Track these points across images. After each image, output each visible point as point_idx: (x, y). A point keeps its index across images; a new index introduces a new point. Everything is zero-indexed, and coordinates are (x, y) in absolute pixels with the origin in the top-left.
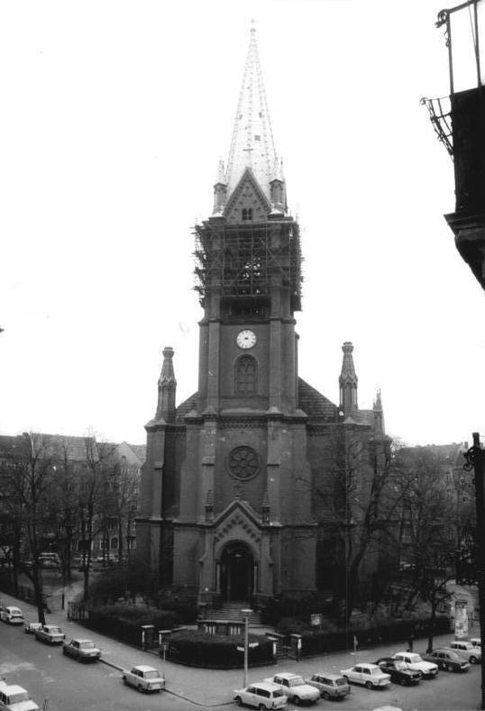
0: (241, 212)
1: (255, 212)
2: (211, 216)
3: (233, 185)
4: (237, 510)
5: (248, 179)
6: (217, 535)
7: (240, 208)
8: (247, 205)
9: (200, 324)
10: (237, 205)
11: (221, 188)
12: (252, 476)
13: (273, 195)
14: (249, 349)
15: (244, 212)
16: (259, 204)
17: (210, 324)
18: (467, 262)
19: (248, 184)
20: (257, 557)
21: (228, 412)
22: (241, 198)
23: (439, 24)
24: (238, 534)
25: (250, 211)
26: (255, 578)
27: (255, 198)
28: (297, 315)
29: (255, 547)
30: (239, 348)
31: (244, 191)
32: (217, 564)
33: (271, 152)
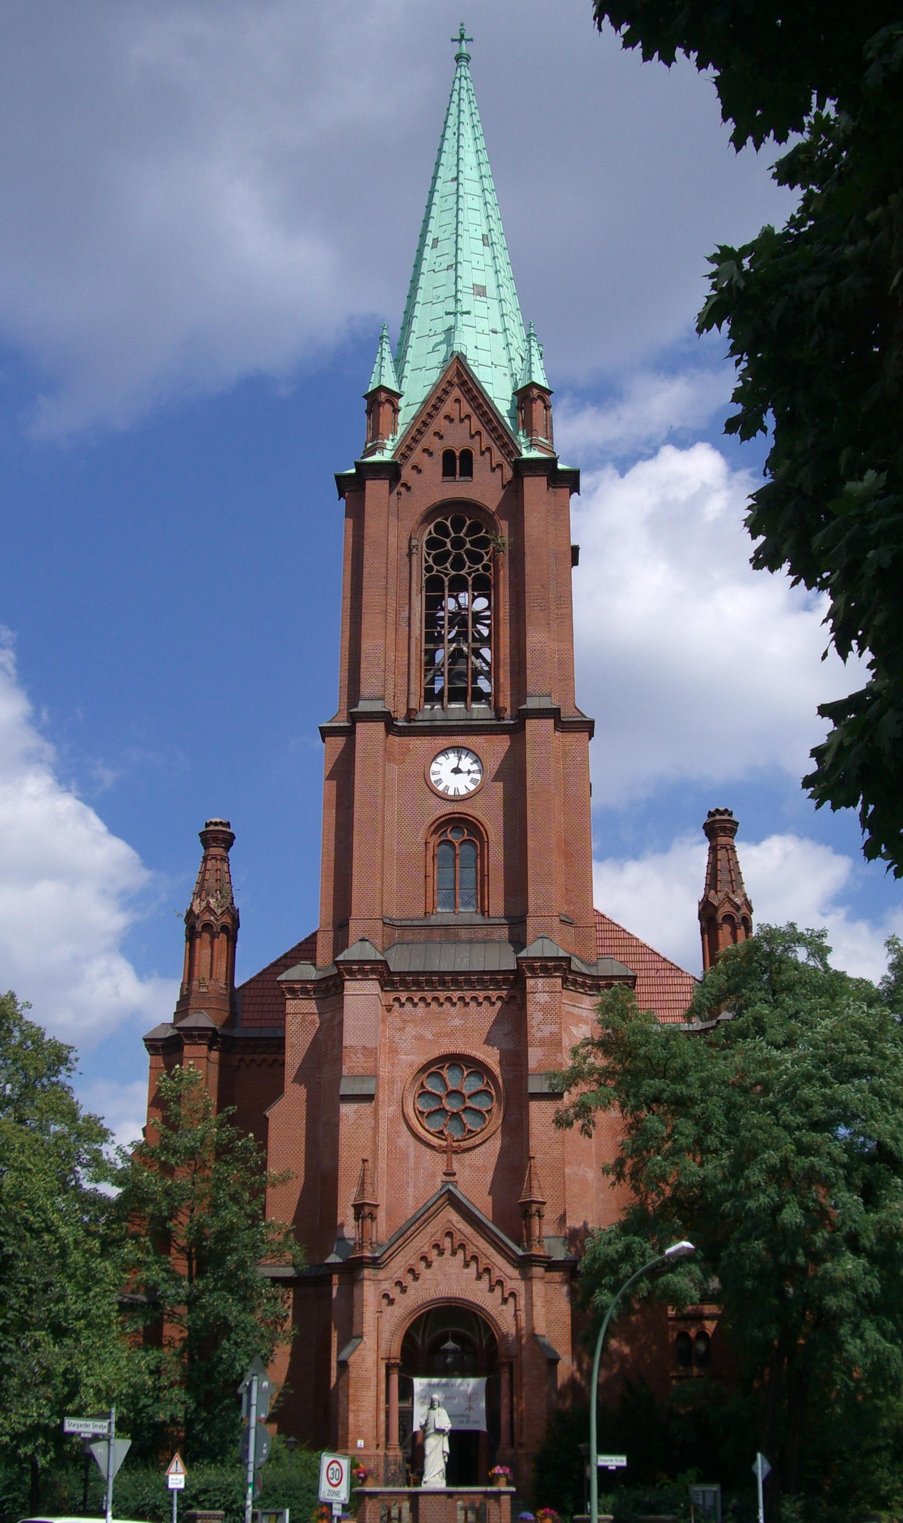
6: (387, 1286)
7: (439, 447)
8: (457, 438)
10: (428, 440)
15: (448, 456)
16: (487, 440)
17: (361, 728)
19: (456, 392)
21: (398, 962)
22: (438, 423)
25: (467, 456)
27: (476, 424)
32: (388, 1367)
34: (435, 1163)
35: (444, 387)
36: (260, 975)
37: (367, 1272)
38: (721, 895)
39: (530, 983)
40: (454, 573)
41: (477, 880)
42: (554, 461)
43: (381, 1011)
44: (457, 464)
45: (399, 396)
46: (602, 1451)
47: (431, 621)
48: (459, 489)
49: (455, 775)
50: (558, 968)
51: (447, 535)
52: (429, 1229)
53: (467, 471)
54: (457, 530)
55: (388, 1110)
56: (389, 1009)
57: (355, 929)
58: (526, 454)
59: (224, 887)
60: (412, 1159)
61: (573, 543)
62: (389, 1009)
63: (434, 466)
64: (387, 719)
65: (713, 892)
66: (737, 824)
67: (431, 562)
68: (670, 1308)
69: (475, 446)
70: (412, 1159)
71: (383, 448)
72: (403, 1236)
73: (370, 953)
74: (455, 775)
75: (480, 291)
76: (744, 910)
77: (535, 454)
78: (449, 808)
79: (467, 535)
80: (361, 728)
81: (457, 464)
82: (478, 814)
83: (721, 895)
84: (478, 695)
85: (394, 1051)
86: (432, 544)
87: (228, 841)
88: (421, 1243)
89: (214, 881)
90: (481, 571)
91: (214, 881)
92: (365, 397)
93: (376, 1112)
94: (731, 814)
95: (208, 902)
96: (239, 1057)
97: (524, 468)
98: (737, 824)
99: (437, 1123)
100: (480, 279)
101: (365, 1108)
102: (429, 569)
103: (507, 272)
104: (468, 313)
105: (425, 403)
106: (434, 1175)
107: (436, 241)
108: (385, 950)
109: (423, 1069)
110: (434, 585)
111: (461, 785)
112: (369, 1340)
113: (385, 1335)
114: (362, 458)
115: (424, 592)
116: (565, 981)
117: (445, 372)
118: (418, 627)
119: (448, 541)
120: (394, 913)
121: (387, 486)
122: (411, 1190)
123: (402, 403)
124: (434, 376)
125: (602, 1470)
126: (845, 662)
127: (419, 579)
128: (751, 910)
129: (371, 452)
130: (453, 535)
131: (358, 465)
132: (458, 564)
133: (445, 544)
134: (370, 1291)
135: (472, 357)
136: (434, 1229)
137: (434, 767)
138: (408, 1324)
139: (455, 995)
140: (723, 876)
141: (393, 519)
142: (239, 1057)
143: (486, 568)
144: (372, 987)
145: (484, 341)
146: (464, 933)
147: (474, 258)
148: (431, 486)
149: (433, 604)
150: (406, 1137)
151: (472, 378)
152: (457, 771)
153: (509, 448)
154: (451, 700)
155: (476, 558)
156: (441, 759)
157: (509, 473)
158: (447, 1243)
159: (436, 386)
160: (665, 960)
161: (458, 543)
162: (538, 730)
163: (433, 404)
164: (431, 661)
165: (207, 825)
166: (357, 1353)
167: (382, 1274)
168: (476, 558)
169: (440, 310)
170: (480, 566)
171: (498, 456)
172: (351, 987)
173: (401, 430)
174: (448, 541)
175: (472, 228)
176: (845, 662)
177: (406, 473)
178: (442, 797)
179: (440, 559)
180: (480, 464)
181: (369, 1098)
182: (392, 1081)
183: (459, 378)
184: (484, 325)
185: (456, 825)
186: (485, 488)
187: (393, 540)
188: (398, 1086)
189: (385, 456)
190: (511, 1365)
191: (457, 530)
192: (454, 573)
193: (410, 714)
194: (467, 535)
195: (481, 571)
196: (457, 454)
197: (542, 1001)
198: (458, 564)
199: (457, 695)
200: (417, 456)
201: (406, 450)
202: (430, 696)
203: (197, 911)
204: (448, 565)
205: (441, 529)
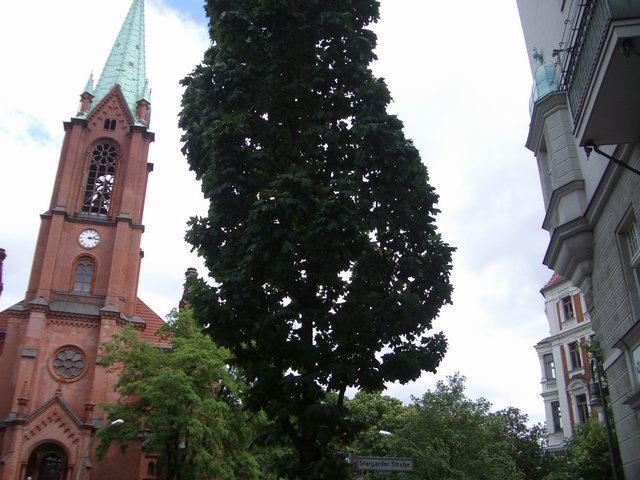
0: (104, 122)
1: (118, 123)
2: (74, 116)
3: (99, 97)
4: (57, 407)
5: (116, 93)
6: (27, 433)
7: (104, 118)
8: (112, 116)
9: (43, 217)
10: (101, 114)
11: (86, 97)
12: (75, 380)
13: (138, 113)
14: (90, 249)
15: (107, 121)
16: (122, 118)
17: (55, 217)
18: (412, 155)
19: (114, 98)
20: (73, 460)
21: (55, 308)
22: (106, 109)
23: (554, 55)
24: (53, 432)
25: (114, 122)
26: (605, 46)
27: (120, 111)
28: (403, 130)
29: (72, 449)
30: (79, 244)
31: (109, 104)
32: (22, 466)
33: (142, 80)
34: (56, 385)
37: (19, 427)
39: (103, 321)
41: (552, 113)
43: (44, 325)
44: (110, 125)
48: (108, 134)
49: (89, 239)
50: (115, 316)
53: (113, 128)
55: (41, 364)
56: (48, 325)
57: (39, 293)
58: (136, 124)
61: (149, 161)
62: (48, 325)
63: (101, 124)
64: (65, 215)
68: (349, 127)
69: (118, 120)
72: (37, 414)
73: (42, 302)
74: (89, 239)
75: (131, 64)
77: (139, 125)
80: (55, 217)
81: (110, 125)
84: (104, 211)
85: (47, 341)
86: (95, 153)
88: (44, 417)
93: (35, 364)
97: (134, 129)
99: (60, 372)
100: (132, 60)
101: (31, 363)
108: (50, 302)
109: (58, 349)
111: (91, 244)
112: (16, 454)
116: (117, 323)
117: (112, 91)
118: (85, 182)
120: (56, 288)
123: (93, 99)
124: (107, 92)
126: (588, 156)
127: (88, 164)
132: (104, 161)
134: (19, 434)
135: (123, 87)
136: (49, 412)
137: (81, 236)
139: (75, 323)
141: (82, 142)
144: (42, 316)
146: (82, 300)
150: (47, 377)
151: (121, 94)
152: (90, 238)
153: (130, 119)
155: (111, 160)
156: (84, 233)
157: (128, 130)
158: (54, 418)
162: (123, 227)
167: (26, 428)
171: (125, 124)
172: (33, 315)
176: (588, 156)
177: (90, 125)
178: (83, 247)
179: (97, 159)
180: (118, 126)
181: (33, 357)
182: (45, 354)
184: (131, 77)
185: (86, 258)
186: (118, 135)
187: (80, 150)
188: (47, 356)
190: (72, 468)
193: (76, 214)
198: (104, 161)
199: (95, 210)
202: (85, 209)
205: (100, 148)
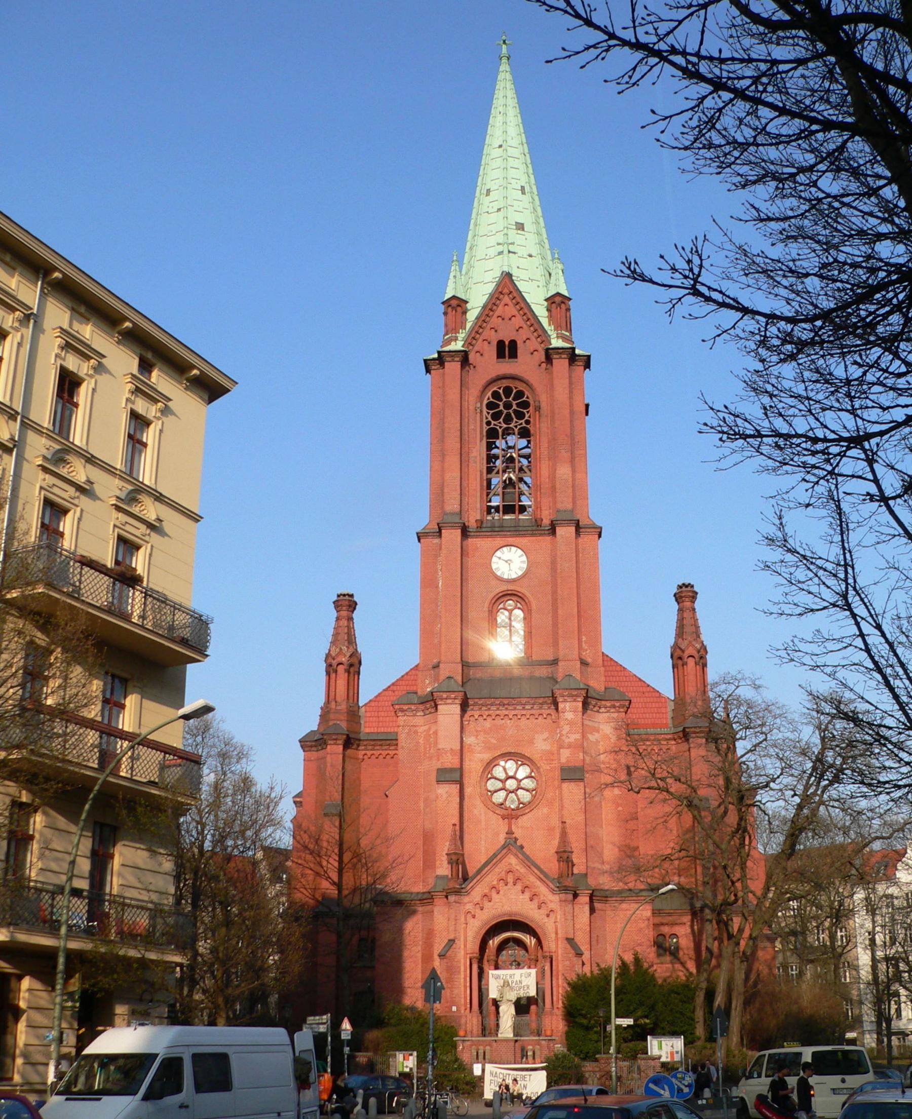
7: (494, 338)
10: (487, 333)
15: (501, 344)
22: (494, 321)
25: (513, 343)
35: (496, 296)
36: (376, 697)
38: (686, 642)
40: (505, 426)
42: (573, 349)
45: (466, 302)
46: (617, 1016)
47: (491, 458)
51: (501, 400)
52: (497, 870)
53: (514, 354)
54: (507, 396)
59: (351, 640)
60: (483, 823)
65: (680, 640)
66: (697, 593)
67: (490, 419)
70: (483, 823)
71: (456, 339)
76: (702, 652)
78: (504, 587)
79: (514, 399)
81: (507, 350)
82: (524, 591)
83: (686, 642)
87: (353, 606)
89: (345, 634)
90: (524, 425)
91: (345, 634)
92: (443, 303)
94: (692, 586)
95: (341, 649)
96: (364, 752)
98: (697, 593)
102: (488, 423)
103: (533, 181)
104: (514, 253)
105: (484, 307)
106: (497, 834)
107: (488, 191)
110: (492, 434)
113: (470, 939)
114: (442, 347)
115: (485, 439)
119: (501, 403)
121: (459, 366)
122: (483, 842)
124: (490, 288)
125: (618, 1027)
128: (706, 652)
129: (448, 342)
130: (504, 400)
131: (439, 353)
132: (508, 419)
133: (498, 406)
138: (484, 931)
140: (688, 629)
142: (364, 752)
143: (528, 422)
145: (525, 263)
147: (516, 203)
148: (488, 366)
149: (490, 446)
154: (505, 513)
155: (520, 416)
159: (492, 296)
160: (648, 686)
161: (508, 406)
163: (489, 308)
164: (489, 482)
165: (338, 596)
166: (451, 950)
168: (520, 416)
169: (492, 241)
170: (523, 421)
173: (469, 325)
174: (501, 403)
175: (513, 181)
177: (472, 357)
178: (498, 578)
179: (496, 417)
183: (506, 288)
189: (458, 346)
191: (507, 396)
192: (505, 426)
194: (514, 399)
195: (524, 425)
196: (507, 343)
197: (569, 718)
200: (479, 345)
201: (471, 340)
203: (333, 654)
204: (501, 420)
